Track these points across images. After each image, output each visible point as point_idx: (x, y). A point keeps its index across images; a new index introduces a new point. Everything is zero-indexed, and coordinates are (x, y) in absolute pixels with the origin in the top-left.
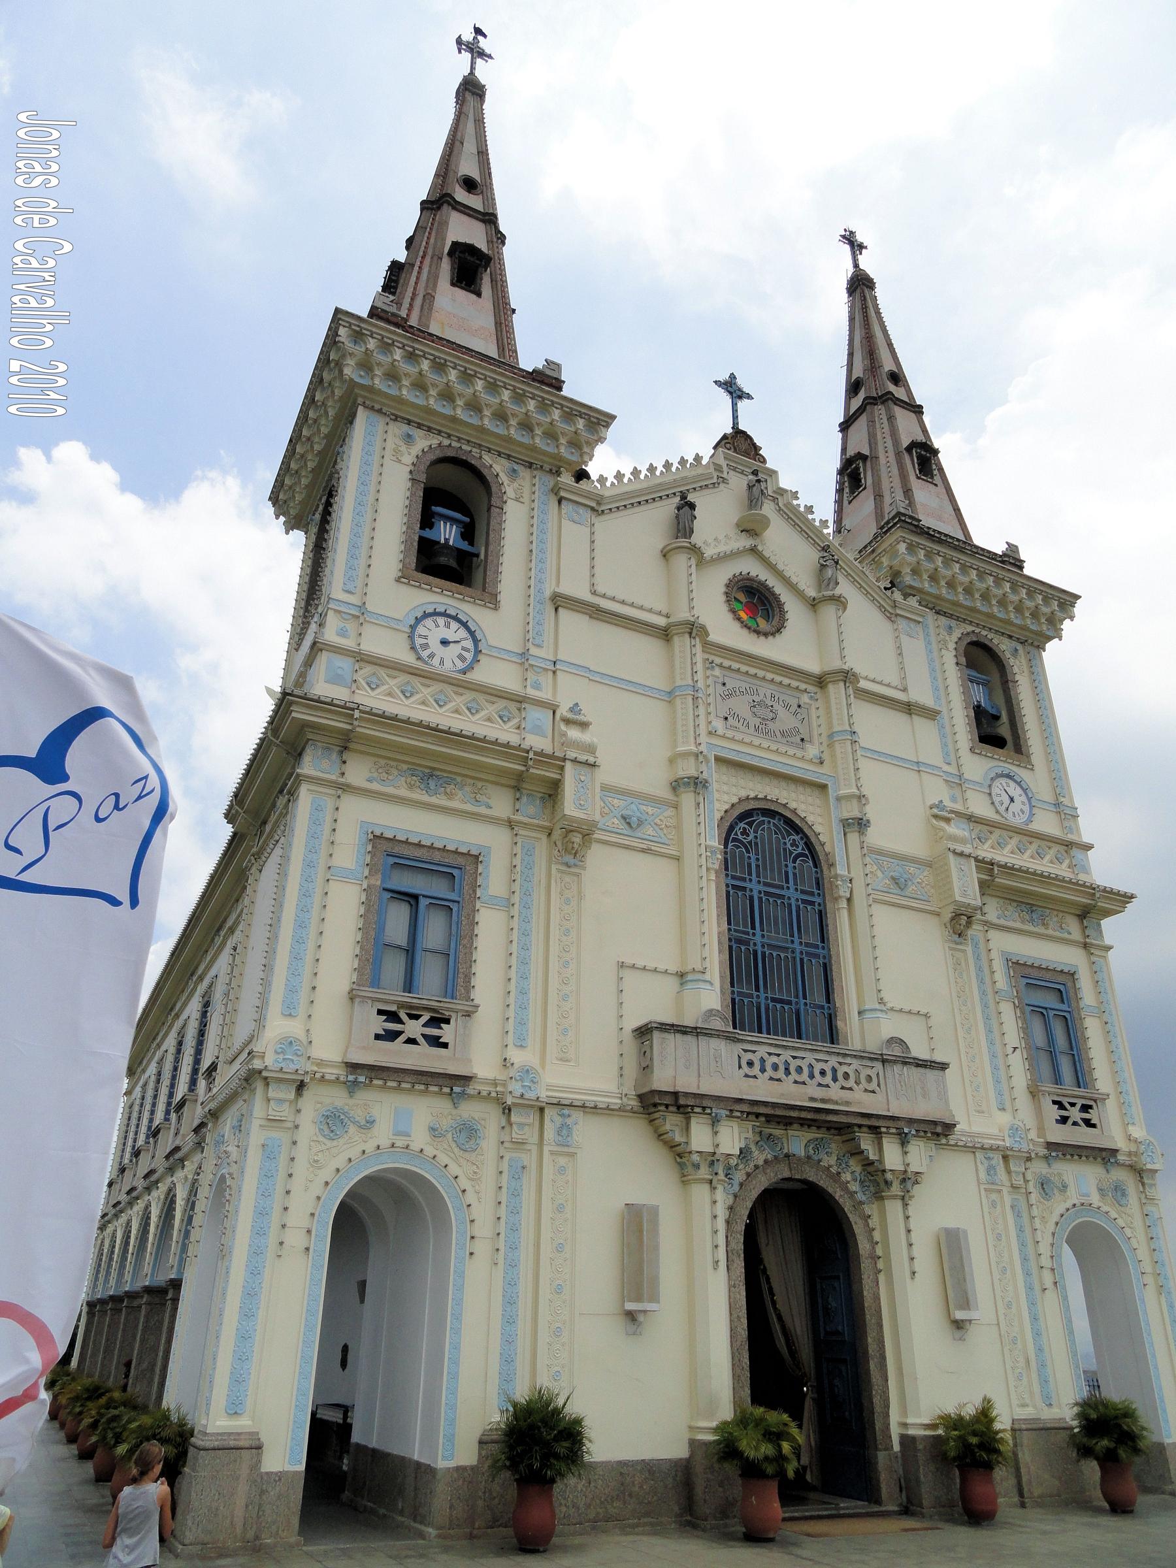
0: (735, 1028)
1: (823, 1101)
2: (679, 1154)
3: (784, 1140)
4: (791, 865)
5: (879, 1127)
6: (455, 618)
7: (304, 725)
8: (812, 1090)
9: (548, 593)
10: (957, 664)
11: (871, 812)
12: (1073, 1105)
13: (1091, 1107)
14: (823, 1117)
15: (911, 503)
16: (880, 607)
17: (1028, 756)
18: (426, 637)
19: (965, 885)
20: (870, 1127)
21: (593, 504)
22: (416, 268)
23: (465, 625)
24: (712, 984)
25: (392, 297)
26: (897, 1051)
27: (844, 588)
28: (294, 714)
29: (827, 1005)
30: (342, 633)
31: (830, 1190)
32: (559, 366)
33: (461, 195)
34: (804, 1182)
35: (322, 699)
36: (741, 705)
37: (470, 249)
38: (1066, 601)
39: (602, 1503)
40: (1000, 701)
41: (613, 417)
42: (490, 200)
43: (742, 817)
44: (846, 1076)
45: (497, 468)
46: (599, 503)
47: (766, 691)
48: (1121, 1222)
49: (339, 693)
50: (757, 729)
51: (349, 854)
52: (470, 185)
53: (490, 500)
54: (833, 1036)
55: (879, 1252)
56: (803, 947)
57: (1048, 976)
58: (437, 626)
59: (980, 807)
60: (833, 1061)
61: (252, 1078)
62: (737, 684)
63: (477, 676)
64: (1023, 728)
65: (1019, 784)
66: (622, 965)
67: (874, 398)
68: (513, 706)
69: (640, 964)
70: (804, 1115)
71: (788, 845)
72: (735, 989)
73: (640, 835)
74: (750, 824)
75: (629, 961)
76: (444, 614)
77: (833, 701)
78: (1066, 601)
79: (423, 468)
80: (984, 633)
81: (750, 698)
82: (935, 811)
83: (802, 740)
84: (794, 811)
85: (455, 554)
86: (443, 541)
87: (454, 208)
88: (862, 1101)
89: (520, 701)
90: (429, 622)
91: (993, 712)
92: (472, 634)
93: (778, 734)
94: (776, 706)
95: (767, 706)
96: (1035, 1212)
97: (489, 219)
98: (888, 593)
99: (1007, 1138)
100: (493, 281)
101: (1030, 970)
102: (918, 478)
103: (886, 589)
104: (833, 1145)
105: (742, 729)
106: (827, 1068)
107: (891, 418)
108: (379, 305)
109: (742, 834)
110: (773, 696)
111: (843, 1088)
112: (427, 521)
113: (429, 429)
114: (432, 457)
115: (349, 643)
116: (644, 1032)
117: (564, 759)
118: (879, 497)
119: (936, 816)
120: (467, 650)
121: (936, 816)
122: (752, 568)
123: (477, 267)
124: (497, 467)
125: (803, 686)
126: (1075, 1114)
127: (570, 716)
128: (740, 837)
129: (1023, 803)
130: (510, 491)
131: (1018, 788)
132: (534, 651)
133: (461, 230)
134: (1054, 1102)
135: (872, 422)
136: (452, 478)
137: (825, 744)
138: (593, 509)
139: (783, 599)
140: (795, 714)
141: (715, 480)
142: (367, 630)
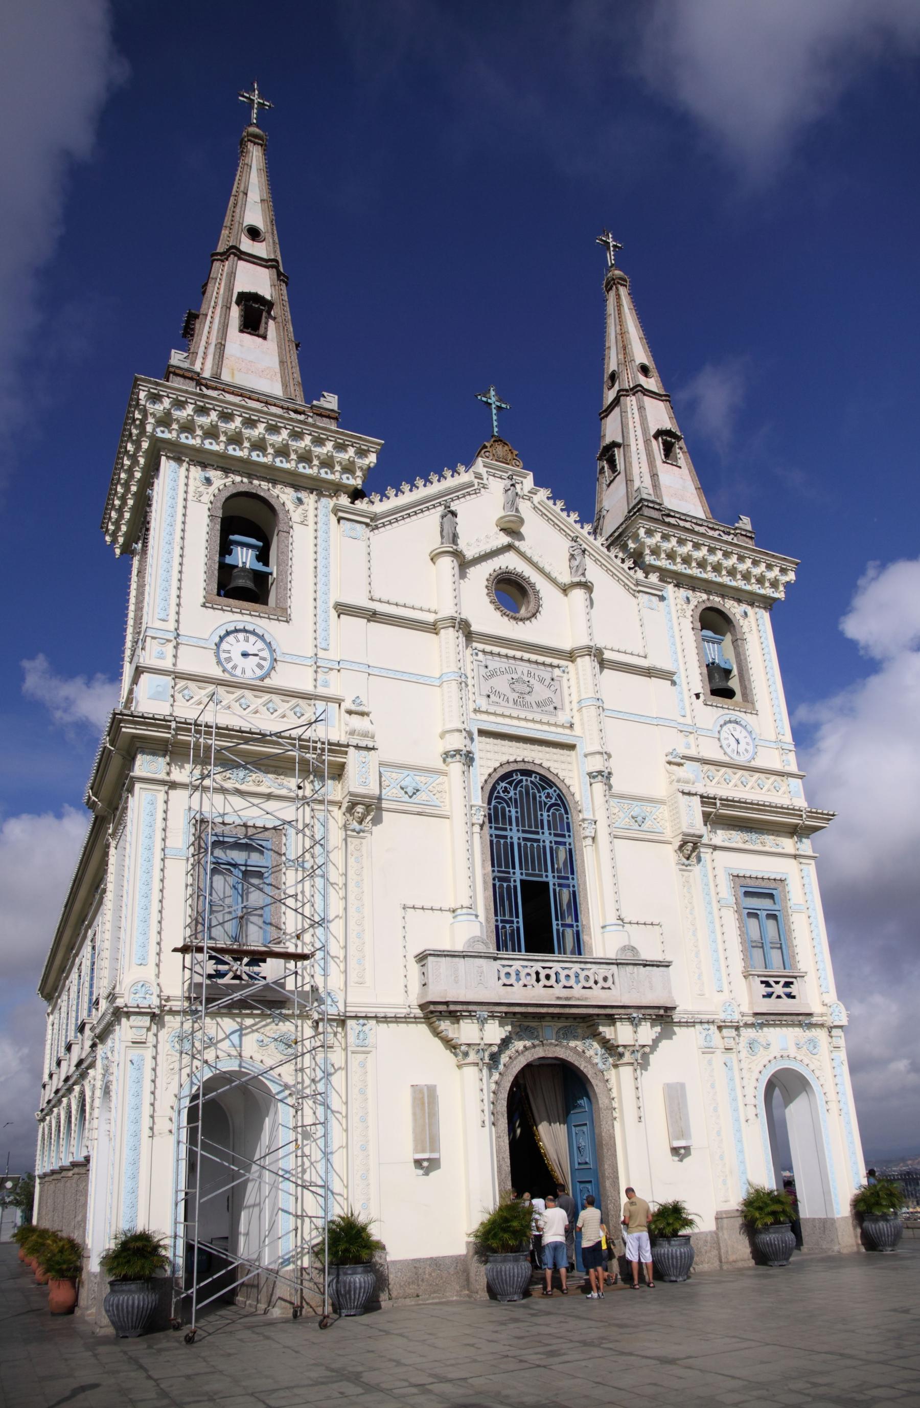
0: (498, 949)
1: (567, 999)
2: (451, 1045)
3: (540, 1030)
4: (545, 814)
5: (614, 1015)
6: (253, 633)
7: (134, 737)
8: (558, 991)
9: (332, 604)
11: (614, 765)
12: (777, 983)
13: (792, 983)
14: (567, 1011)
15: (656, 485)
16: (625, 585)
18: (229, 652)
19: (691, 817)
20: (606, 1015)
21: (368, 521)
22: (209, 318)
23: (262, 637)
24: (477, 916)
26: (629, 956)
27: (594, 573)
28: (124, 730)
29: (575, 924)
31: (576, 1063)
34: (556, 1058)
35: (146, 715)
36: (501, 684)
39: (401, 1286)
40: (730, 655)
43: (503, 778)
44: (587, 978)
45: (283, 498)
46: (372, 519)
47: (523, 668)
48: (812, 1067)
49: (161, 709)
50: (515, 702)
51: (181, 837)
54: (578, 948)
55: (615, 1105)
56: (556, 879)
57: (763, 884)
58: (238, 641)
60: (576, 967)
61: (119, 1014)
63: (274, 681)
64: (749, 680)
65: (745, 727)
67: (627, 391)
70: (551, 1010)
71: (543, 798)
72: (499, 918)
73: (415, 801)
74: (510, 783)
75: (410, 903)
76: (245, 631)
77: (580, 669)
79: (219, 504)
81: (509, 676)
82: (670, 758)
83: (555, 708)
85: (251, 576)
86: (240, 565)
88: (598, 996)
90: (231, 638)
91: (727, 667)
92: (269, 645)
94: (532, 681)
95: (524, 682)
96: (744, 1065)
98: (632, 572)
101: (748, 880)
102: (664, 462)
103: (630, 568)
104: (579, 1031)
106: (571, 973)
107: (641, 408)
109: (504, 792)
110: (529, 673)
111: (584, 988)
112: (225, 548)
114: (227, 494)
115: (167, 664)
116: (422, 958)
117: (348, 746)
118: (629, 481)
119: (670, 763)
120: (264, 659)
121: (670, 763)
122: (510, 562)
124: (284, 496)
126: (779, 989)
127: (354, 708)
128: (502, 795)
129: (748, 744)
130: (296, 515)
131: (744, 731)
132: (321, 654)
134: (762, 982)
135: (623, 413)
136: (247, 510)
137: (575, 710)
139: (533, 580)
140: (549, 686)
141: (476, 487)
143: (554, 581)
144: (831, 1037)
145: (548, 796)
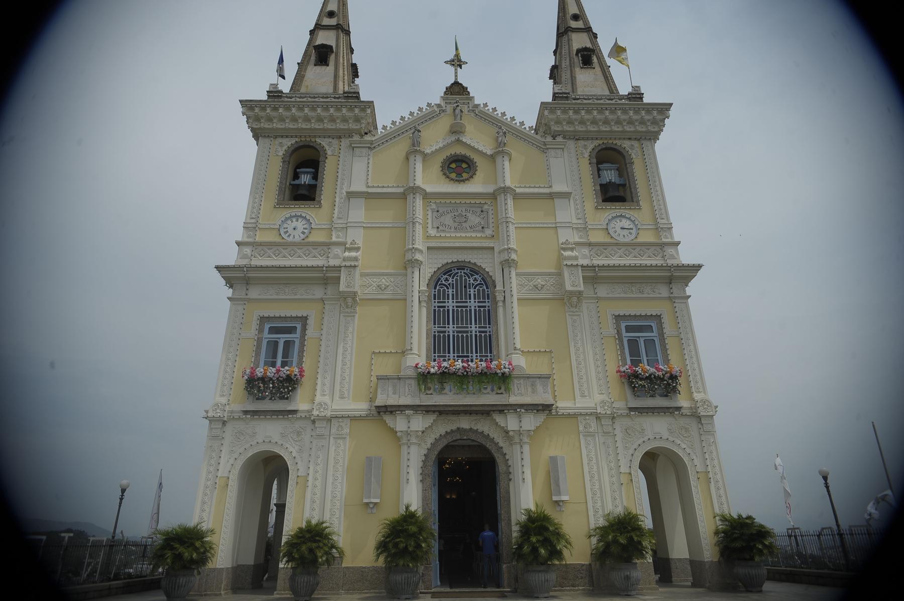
17: (638, 202)
19: (573, 282)
30: (338, 237)
32: (639, 87)
33: (574, 24)
36: (448, 220)
38: (664, 109)
42: (586, 22)
45: (323, 143)
50: (455, 228)
52: (576, 17)
59: (598, 237)
63: (311, 239)
66: (374, 353)
69: (382, 351)
74: (450, 275)
80: (610, 142)
84: (475, 264)
89: (329, 245)
94: (468, 214)
97: (588, 29)
99: (599, 408)
100: (598, 58)
108: (556, 91)
117: (340, 267)
133: (579, 41)
138: (369, 148)
142: (258, 233)
144: (702, 424)
145: (475, 280)
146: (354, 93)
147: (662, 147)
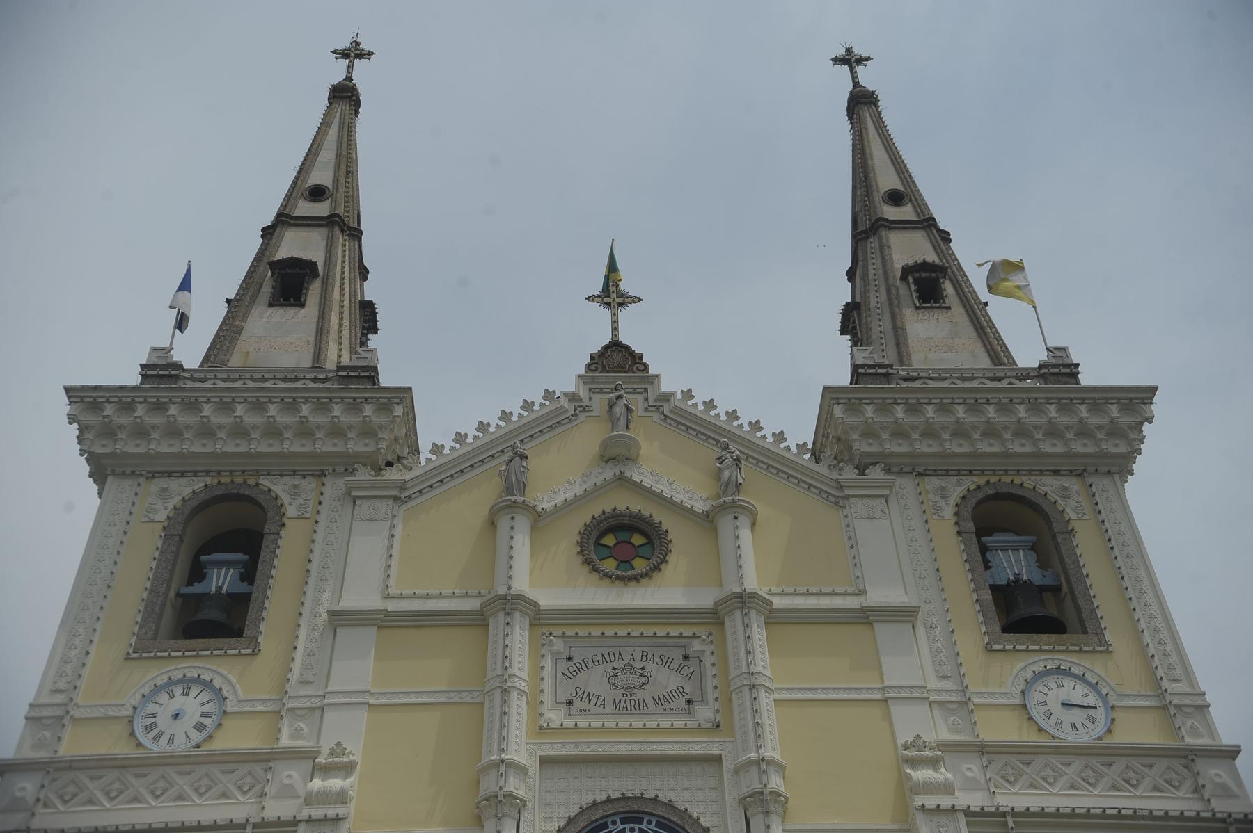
10: (959, 533)
17: (1100, 633)
21: (395, 493)
25: (870, 349)
30: (296, 735)
32: (1064, 349)
35: (220, 822)
37: (924, 266)
38: (1136, 401)
41: (1153, 390)
50: (616, 705)
52: (895, 198)
53: (1051, 528)
59: (1002, 729)
62: (589, 653)
68: (257, 769)
78: (1136, 401)
80: (1006, 479)
84: (670, 805)
87: (890, 229)
93: (650, 703)
94: (650, 667)
97: (927, 223)
100: (957, 286)
105: (594, 710)
110: (644, 655)
113: (959, 473)
123: (937, 279)
125: (687, 631)
133: (907, 249)
139: (656, 519)
143: (689, 512)
146: (365, 368)
147: (1134, 489)
